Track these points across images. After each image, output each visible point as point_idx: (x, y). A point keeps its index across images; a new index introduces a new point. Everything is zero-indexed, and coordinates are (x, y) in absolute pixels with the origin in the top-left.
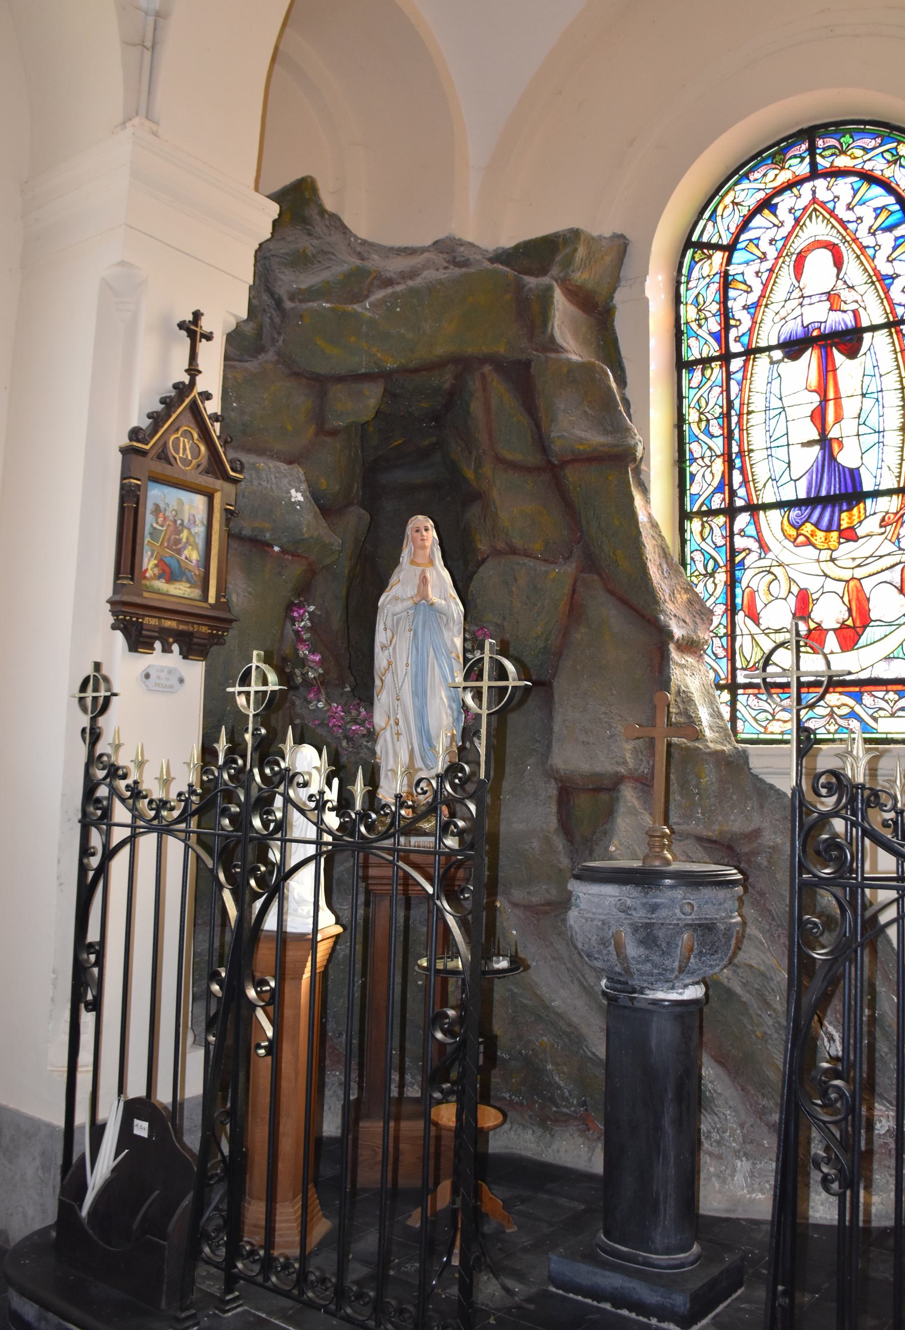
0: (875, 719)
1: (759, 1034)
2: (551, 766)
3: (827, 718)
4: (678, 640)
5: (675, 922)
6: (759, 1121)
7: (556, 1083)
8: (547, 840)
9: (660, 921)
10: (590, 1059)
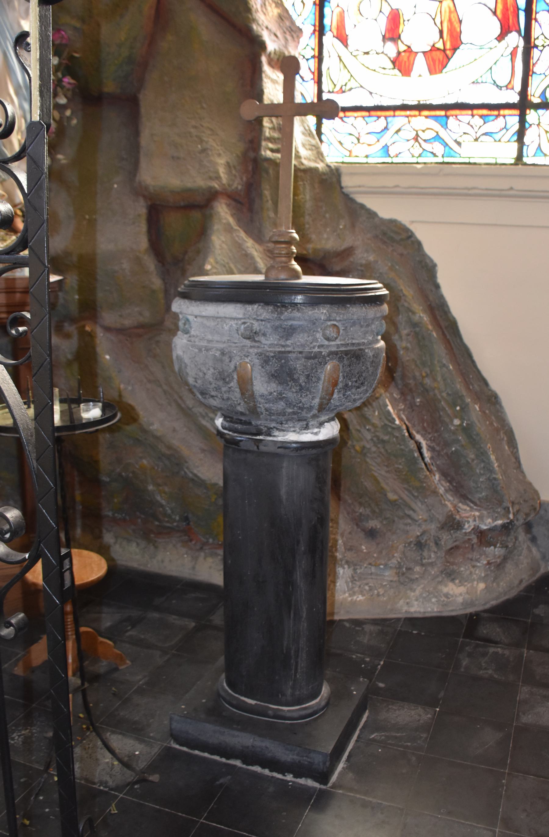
0: (459, 144)
1: (358, 448)
2: (140, 183)
3: (412, 142)
4: (270, 54)
5: (316, 349)
6: (355, 527)
7: (157, 501)
8: (138, 260)
9: (297, 349)
10: (193, 480)
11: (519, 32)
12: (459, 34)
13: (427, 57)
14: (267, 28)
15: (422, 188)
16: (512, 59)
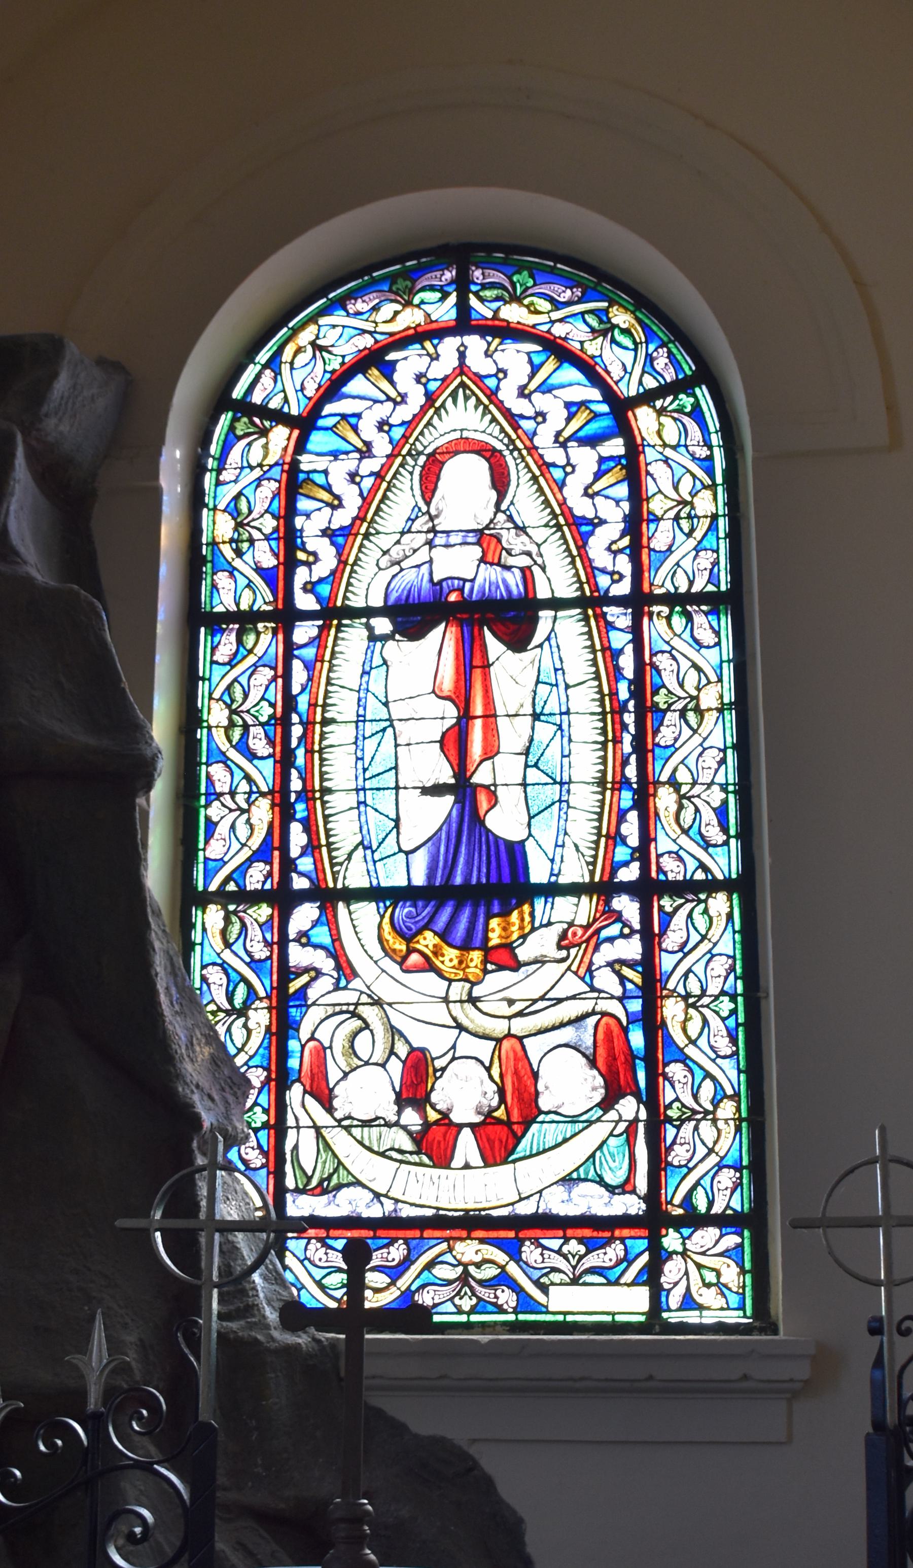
11: (637, 1094)
12: (533, 1097)
13: (478, 1135)
14: (197, 1086)
15: (491, 1380)
16: (628, 1141)
